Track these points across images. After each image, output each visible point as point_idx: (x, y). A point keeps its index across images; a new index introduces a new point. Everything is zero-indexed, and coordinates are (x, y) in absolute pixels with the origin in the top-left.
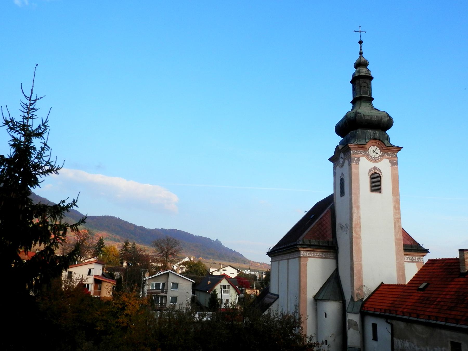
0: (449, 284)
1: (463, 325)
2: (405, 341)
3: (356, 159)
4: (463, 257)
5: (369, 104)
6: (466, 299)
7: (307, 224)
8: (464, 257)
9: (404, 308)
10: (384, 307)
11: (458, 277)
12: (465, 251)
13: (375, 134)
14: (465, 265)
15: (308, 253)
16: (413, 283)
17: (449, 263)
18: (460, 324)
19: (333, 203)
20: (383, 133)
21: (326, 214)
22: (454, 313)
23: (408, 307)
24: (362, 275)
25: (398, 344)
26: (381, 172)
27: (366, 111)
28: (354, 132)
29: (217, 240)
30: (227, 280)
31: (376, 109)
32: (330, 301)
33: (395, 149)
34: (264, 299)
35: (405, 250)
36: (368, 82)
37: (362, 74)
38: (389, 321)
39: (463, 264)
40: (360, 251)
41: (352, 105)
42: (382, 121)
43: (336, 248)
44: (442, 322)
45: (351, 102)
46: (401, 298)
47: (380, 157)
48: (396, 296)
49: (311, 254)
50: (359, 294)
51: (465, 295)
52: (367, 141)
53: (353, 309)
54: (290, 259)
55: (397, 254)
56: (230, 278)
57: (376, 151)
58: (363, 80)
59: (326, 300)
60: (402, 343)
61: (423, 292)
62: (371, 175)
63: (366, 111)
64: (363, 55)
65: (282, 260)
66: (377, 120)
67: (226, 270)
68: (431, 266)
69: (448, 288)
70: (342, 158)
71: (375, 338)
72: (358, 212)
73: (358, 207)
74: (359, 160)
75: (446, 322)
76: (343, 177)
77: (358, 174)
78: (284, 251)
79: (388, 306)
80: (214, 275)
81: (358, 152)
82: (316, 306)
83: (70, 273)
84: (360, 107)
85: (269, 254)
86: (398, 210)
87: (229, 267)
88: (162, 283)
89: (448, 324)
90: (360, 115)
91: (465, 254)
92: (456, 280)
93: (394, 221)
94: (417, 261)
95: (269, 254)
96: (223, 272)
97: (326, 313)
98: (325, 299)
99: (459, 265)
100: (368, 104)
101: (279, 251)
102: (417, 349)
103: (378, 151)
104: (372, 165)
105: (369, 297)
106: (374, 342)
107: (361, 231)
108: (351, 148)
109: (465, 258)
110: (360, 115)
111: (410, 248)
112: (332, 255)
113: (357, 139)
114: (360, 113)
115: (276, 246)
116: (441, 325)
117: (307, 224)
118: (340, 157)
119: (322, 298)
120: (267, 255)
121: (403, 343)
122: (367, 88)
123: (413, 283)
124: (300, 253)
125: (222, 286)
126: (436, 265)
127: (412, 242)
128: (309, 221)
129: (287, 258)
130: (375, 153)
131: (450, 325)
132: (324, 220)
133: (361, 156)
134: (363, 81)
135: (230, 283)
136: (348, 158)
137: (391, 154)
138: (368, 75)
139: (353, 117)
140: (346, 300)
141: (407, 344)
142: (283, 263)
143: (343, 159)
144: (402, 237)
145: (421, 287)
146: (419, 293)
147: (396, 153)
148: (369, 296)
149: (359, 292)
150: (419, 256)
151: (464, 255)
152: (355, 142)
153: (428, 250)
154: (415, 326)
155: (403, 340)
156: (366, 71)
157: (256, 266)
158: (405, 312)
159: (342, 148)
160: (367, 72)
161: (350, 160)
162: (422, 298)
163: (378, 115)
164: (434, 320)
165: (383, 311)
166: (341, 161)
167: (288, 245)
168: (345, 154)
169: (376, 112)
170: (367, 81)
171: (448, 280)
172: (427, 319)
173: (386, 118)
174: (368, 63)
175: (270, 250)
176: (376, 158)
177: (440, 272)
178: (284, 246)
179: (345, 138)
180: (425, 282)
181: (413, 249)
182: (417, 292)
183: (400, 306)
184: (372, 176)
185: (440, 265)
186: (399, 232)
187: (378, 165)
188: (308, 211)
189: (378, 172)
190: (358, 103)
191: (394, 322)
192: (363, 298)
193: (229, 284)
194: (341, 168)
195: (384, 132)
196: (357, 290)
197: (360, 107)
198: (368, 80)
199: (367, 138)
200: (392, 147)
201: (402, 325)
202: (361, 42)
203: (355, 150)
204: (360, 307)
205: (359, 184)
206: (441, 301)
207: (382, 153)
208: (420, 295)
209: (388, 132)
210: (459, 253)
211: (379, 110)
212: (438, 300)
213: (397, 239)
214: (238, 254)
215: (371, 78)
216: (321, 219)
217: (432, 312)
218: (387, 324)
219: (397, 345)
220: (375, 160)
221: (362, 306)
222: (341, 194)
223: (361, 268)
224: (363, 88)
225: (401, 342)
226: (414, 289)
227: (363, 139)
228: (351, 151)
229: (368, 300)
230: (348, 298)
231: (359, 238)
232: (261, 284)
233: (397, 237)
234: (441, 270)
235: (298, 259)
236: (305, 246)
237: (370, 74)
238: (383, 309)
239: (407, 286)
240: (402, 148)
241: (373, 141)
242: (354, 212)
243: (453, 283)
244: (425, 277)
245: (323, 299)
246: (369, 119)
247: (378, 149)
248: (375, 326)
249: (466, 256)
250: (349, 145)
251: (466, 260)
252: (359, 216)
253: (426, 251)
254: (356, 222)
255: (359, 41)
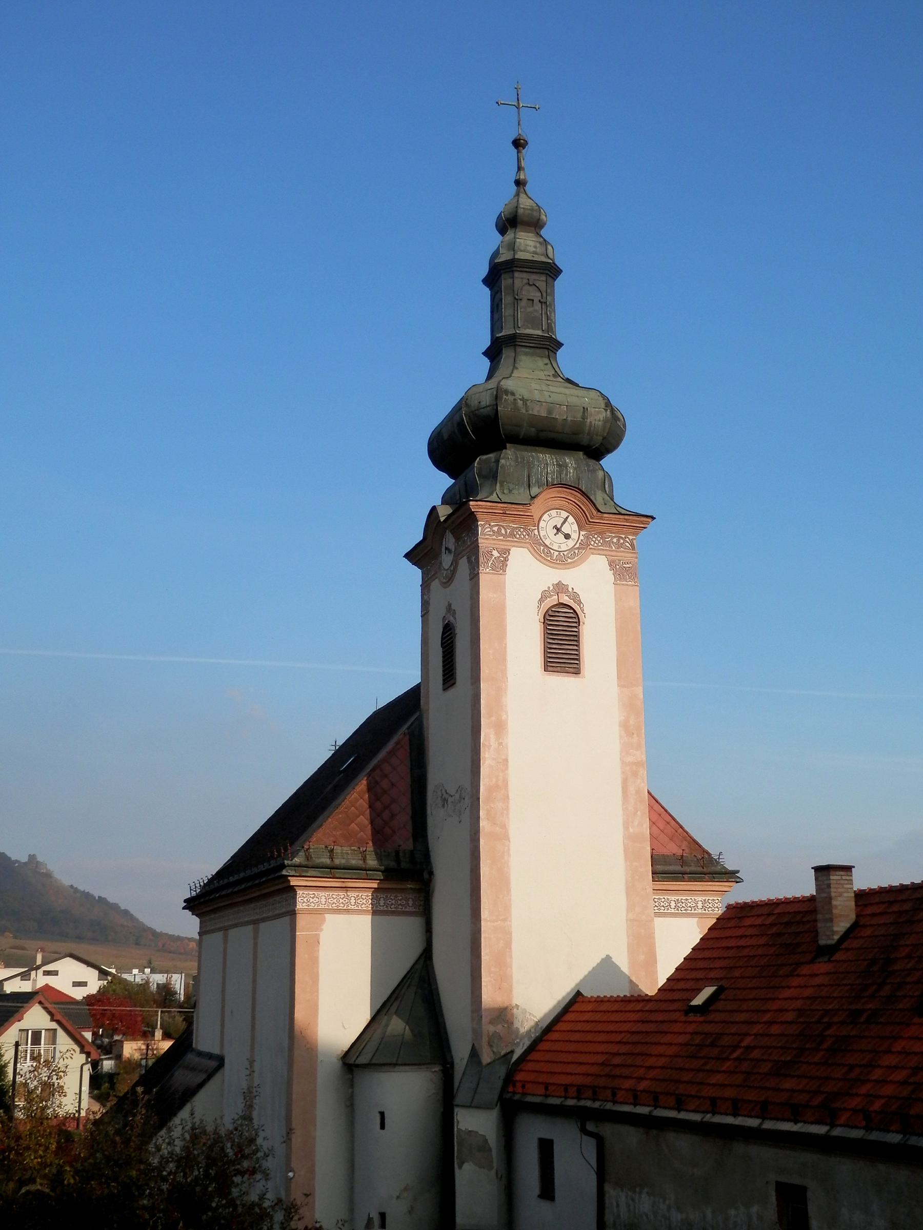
0: (783, 987)
1: (812, 1123)
2: (640, 1193)
3: (496, 554)
4: (827, 890)
5: (546, 361)
6: (828, 1032)
7: (328, 789)
8: (830, 892)
9: (640, 1079)
10: (579, 1080)
11: (812, 961)
12: (832, 873)
13: (562, 466)
14: (831, 920)
15: (322, 894)
16: (673, 990)
17: (789, 913)
18: (805, 1122)
19: (418, 714)
20: (588, 466)
21: (392, 753)
22: (788, 1084)
23: (652, 1074)
24: (511, 968)
25: (618, 1205)
26: (579, 603)
27: (534, 386)
28: (490, 457)
29: (32, 857)
30: (45, 1008)
31: (568, 381)
32: (397, 1068)
33: (627, 520)
34: (172, 1075)
35: (657, 875)
36: (542, 285)
37: (521, 255)
38: (590, 1127)
39: (827, 916)
40: (504, 883)
41: (486, 363)
42: (588, 423)
43: (426, 876)
44: (751, 1117)
45: (485, 354)
46: (633, 1043)
47: (578, 548)
48: (619, 1038)
49: (336, 898)
50: (500, 1038)
51: (826, 1020)
52: (535, 490)
53: (475, 1092)
54: (264, 920)
55: (630, 889)
56: (73, 1001)
57: (566, 529)
58: (525, 275)
59: (384, 1065)
60: (631, 1202)
61: (701, 1019)
62: (547, 611)
63: (534, 386)
64: (527, 188)
65: (236, 926)
66: (569, 419)
67: (55, 973)
68: (735, 927)
69: (778, 999)
70: (450, 551)
71: (547, 1192)
72: (500, 744)
73: (500, 727)
74: (506, 559)
75: (764, 1119)
76: (452, 619)
77: (500, 610)
78: (239, 891)
79: (592, 1075)
80: (8, 992)
81: (503, 531)
82: (350, 1090)
83: (172, 976)
84: (515, 371)
85: (192, 904)
86: (635, 735)
87: (68, 960)
88: (32, 1031)
89: (769, 1125)
90: (511, 398)
91: (832, 882)
92: (805, 970)
93: (623, 773)
94: (700, 911)
95: (192, 904)
96: (41, 980)
97: (382, 1114)
98: (381, 1061)
99: (816, 921)
100: (541, 362)
101: (224, 893)
102: (676, 1217)
103: (571, 527)
104: (548, 576)
105: (533, 1047)
106: (545, 1205)
107: (508, 814)
108: (479, 516)
109: (833, 894)
110: (511, 398)
111: (678, 868)
112: (411, 902)
113: (502, 486)
114: (513, 394)
115: (220, 874)
116: (750, 1129)
117: (328, 789)
118: (443, 550)
119: (372, 1059)
120: (184, 908)
121: (633, 1200)
122: (538, 306)
123: (673, 990)
124: (294, 898)
125: (24, 1034)
126: (748, 922)
127: (685, 845)
128: (337, 779)
129: (252, 918)
130: (560, 536)
131: (803, 1130)
132: (386, 776)
133: (513, 544)
134: (525, 281)
135: (59, 1022)
136: (468, 550)
137: (615, 540)
138: (544, 259)
139: (486, 407)
140: (457, 1060)
141: (645, 1203)
142: (241, 936)
143: (453, 554)
144: (645, 828)
145: (698, 1000)
146: (691, 1022)
147: (631, 537)
148: (534, 1040)
149: (499, 1028)
150: (712, 895)
151: (829, 886)
152: (495, 494)
153: (738, 872)
154: (671, 1136)
155: (635, 1192)
156: (538, 245)
157: (180, 954)
158: (642, 1091)
159: (449, 517)
160: (538, 250)
161: (472, 555)
162: (698, 1040)
163: (574, 400)
164: (727, 1114)
165: (572, 1091)
166: (446, 560)
167: (255, 870)
168: (457, 538)
169: (567, 391)
170: (540, 280)
171: (781, 973)
172: (708, 1112)
173: (598, 413)
174: (543, 217)
175: (198, 891)
176: (565, 553)
177: (759, 946)
178: (242, 875)
179: (461, 478)
180: (708, 981)
181: (688, 869)
182: (683, 1018)
183: (626, 1071)
184: (552, 616)
185: (758, 921)
186: (639, 812)
187: (570, 578)
188: (340, 742)
189: (571, 603)
190: (507, 354)
191: (607, 1130)
192: (512, 1052)
193: (54, 1025)
194: (445, 588)
195: (592, 462)
196: (491, 1022)
197: (512, 373)
198: (543, 278)
199: (533, 480)
200: (620, 514)
201: (631, 1136)
202: (518, 144)
203: (492, 524)
204: (499, 1084)
205: (506, 644)
206: (755, 1047)
207: (587, 537)
208: (691, 1028)
209: (608, 462)
210: (816, 879)
211: (577, 385)
212: (747, 1041)
213: (630, 839)
214: (115, 907)
215: (552, 271)
216: (373, 770)
217: (723, 1086)
218: (585, 1138)
219: (615, 1210)
220: (561, 561)
221: (509, 1080)
222: (444, 680)
223: (508, 944)
224: (523, 303)
225: (626, 1197)
226: (675, 1011)
227: (523, 484)
228: (477, 526)
229: (528, 1058)
230: (460, 1053)
231: (505, 837)
232: (184, 1020)
233: (631, 830)
234: (762, 941)
235: (287, 919)
236: (311, 872)
237: (551, 255)
238: (572, 1085)
239: (656, 1001)
240: (653, 518)
241: (554, 492)
242: (487, 743)
243: (796, 982)
244: (711, 966)
245: (374, 1061)
246: (544, 414)
247: (571, 519)
248: (546, 1148)
249: (837, 886)
250: (471, 503)
251: (834, 903)
252: (503, 757)
253: (731, 876)
254: (494, 780)
255: (513, 139)
